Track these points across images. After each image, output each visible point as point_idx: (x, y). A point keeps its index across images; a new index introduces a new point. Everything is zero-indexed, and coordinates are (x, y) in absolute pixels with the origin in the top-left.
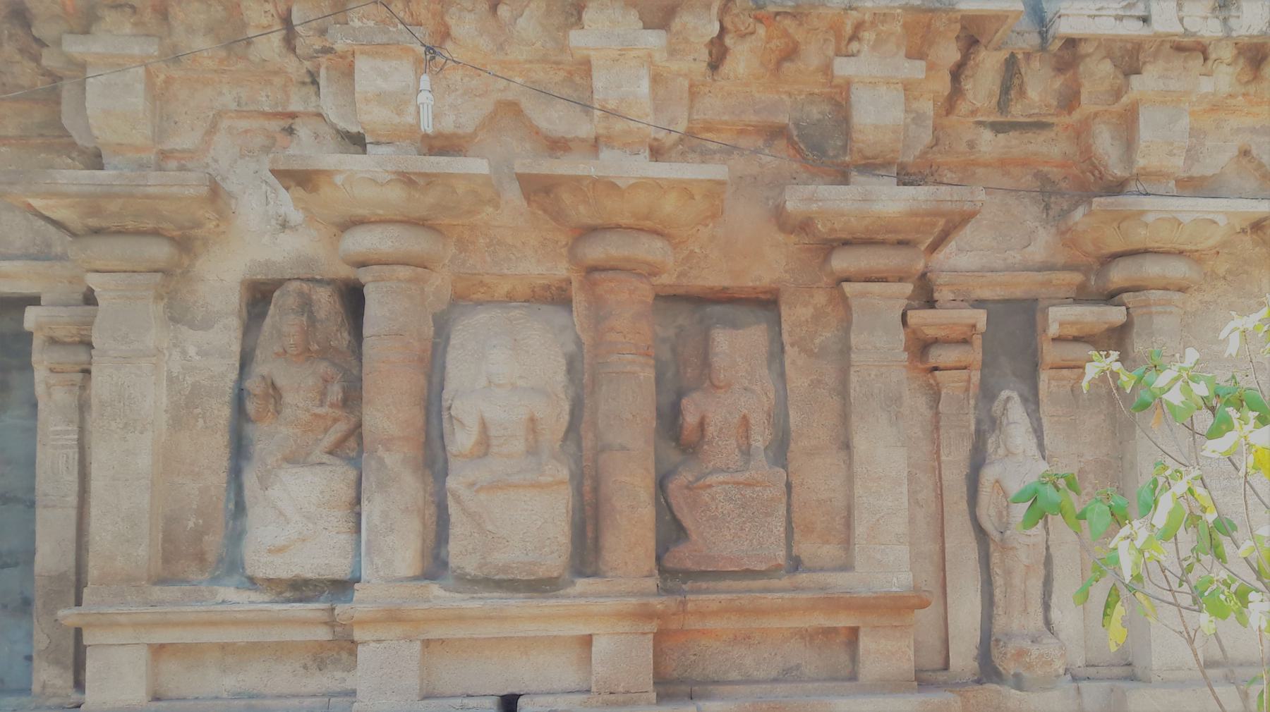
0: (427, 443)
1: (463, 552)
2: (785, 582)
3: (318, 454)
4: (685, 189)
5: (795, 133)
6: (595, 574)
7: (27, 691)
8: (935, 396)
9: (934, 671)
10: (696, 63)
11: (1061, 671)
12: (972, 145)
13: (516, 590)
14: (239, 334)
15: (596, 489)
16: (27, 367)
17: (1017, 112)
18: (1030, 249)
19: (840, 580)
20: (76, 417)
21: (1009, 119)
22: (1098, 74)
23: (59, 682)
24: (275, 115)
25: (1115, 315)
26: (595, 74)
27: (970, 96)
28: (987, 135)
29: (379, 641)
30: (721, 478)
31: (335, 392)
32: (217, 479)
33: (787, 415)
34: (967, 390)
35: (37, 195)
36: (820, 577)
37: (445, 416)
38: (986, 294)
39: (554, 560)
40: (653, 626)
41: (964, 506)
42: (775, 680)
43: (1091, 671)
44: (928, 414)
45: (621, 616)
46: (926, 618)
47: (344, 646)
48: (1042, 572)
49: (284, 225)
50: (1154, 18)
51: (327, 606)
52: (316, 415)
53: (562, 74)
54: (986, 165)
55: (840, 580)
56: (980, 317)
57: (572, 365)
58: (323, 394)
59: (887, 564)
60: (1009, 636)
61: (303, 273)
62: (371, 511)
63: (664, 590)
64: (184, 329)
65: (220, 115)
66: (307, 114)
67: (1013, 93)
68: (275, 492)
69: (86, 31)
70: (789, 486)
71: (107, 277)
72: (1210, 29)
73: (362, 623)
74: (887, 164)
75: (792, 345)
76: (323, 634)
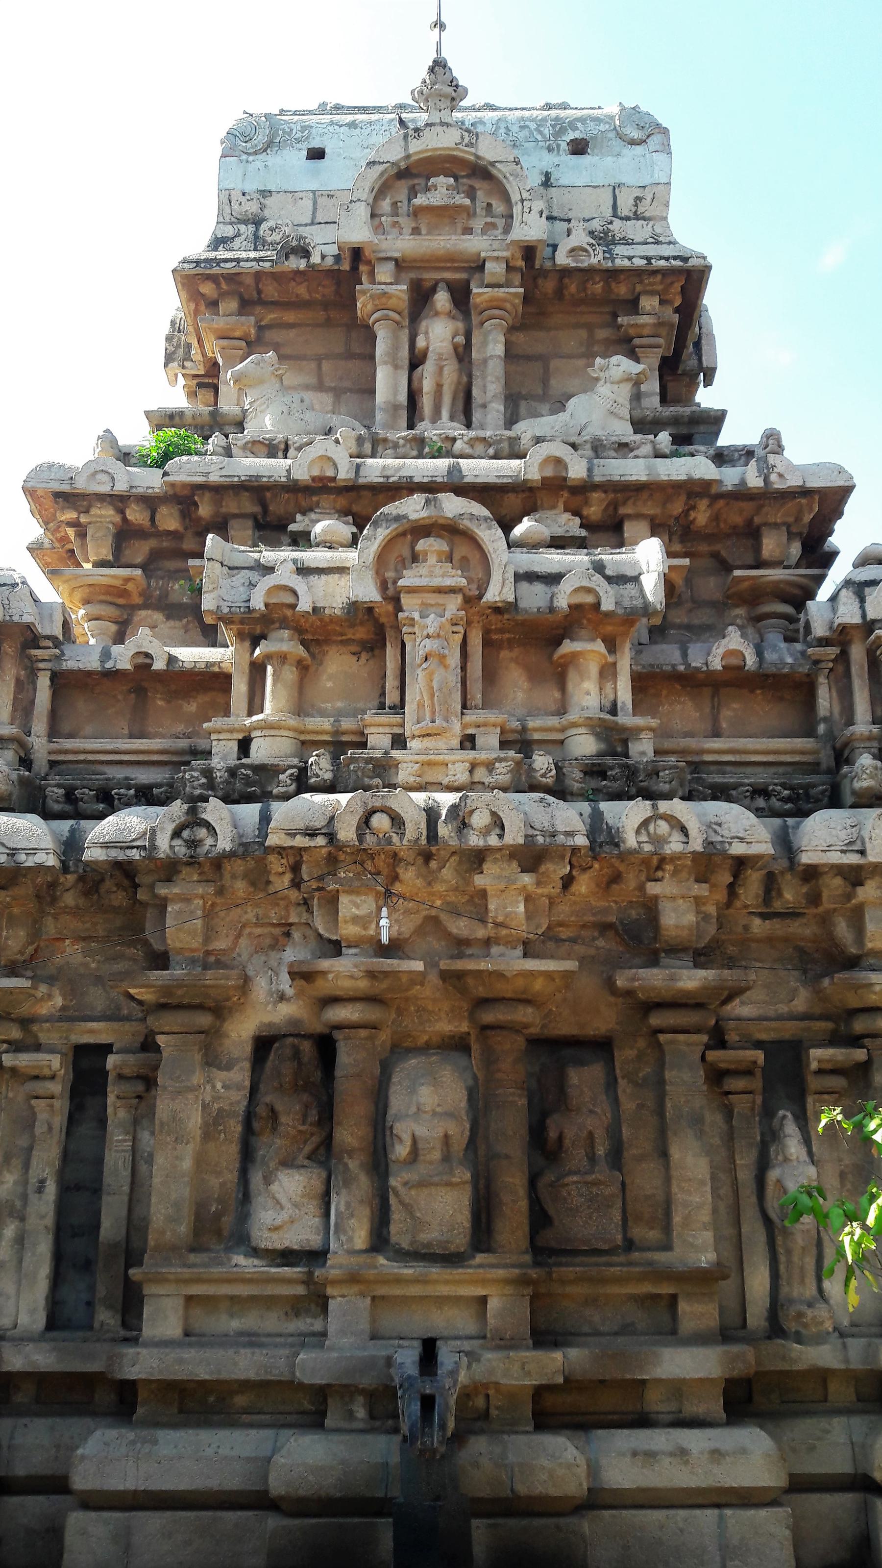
0: (375, 1152)
1: (399, 1231)
2: (622, 1259)
3: (301, 1160)
4: (548, 975)
5: (620, 928)
6: (488, 1250)
7: (91, 1328)
8: (729, 1113)
9: (736, 1329)
10: (553, 888)
11: (830, 1329)
12: (746, 928)
13: (435, 1262)
14: (249, 1074)
15: (488, 1187)
16: (105, 1095)
17: (778, 906)
18: (794, 1003)
19: (661, 1257)
20: (132, 1129)
21: (772, 910)
22: (834, 885)
23: (112, 1322)
24: (279, 925)
25: (860, 1055)
26: (490, 900)
27: (742, 897)
28: (757, 921)
29: (343, 1296)
30: (575, 1179)
31: (313, 1115)
32: (231, 1177)
33: (620, 1131)
34: (753, 1109)
35: (136, 987)
36: (649, 1255)
37: (388, 1133)
38: (764, 1036)
39: (460, 1241)
40: (529, 1291)
41: (754, 1199)
42: (616, 1334)
43: (855, 1330)
44: (725, 1127)
45: (507, 1282)
46: (728, 1286)
47: (318, 1301)
48: (814, 1251)
49: (282, 997)
50: (869, 851)
51: (305, 1269)
52: (300, 1132)
53: (467, 897)
54: (758, 941)
55: (661, 1257)
56: (759, 1056)
57: (472, 1094)
58: (305, 1116)
59: (698, 1245)
60: (791, 1301)
61: (292, 1030)
62: (338, 1203)
63: (537, 1264)
64: (215, 1070)
65: (244, 926)
66: (300, 924)
67: (774, 894)
68: (274, 1187)
69: (169, 880)
70: (623, 1184)
71: (170, 1037)
73: (335, 1282)
74: (684, 950)
75: (623, 1078)
76: (301, 1290)
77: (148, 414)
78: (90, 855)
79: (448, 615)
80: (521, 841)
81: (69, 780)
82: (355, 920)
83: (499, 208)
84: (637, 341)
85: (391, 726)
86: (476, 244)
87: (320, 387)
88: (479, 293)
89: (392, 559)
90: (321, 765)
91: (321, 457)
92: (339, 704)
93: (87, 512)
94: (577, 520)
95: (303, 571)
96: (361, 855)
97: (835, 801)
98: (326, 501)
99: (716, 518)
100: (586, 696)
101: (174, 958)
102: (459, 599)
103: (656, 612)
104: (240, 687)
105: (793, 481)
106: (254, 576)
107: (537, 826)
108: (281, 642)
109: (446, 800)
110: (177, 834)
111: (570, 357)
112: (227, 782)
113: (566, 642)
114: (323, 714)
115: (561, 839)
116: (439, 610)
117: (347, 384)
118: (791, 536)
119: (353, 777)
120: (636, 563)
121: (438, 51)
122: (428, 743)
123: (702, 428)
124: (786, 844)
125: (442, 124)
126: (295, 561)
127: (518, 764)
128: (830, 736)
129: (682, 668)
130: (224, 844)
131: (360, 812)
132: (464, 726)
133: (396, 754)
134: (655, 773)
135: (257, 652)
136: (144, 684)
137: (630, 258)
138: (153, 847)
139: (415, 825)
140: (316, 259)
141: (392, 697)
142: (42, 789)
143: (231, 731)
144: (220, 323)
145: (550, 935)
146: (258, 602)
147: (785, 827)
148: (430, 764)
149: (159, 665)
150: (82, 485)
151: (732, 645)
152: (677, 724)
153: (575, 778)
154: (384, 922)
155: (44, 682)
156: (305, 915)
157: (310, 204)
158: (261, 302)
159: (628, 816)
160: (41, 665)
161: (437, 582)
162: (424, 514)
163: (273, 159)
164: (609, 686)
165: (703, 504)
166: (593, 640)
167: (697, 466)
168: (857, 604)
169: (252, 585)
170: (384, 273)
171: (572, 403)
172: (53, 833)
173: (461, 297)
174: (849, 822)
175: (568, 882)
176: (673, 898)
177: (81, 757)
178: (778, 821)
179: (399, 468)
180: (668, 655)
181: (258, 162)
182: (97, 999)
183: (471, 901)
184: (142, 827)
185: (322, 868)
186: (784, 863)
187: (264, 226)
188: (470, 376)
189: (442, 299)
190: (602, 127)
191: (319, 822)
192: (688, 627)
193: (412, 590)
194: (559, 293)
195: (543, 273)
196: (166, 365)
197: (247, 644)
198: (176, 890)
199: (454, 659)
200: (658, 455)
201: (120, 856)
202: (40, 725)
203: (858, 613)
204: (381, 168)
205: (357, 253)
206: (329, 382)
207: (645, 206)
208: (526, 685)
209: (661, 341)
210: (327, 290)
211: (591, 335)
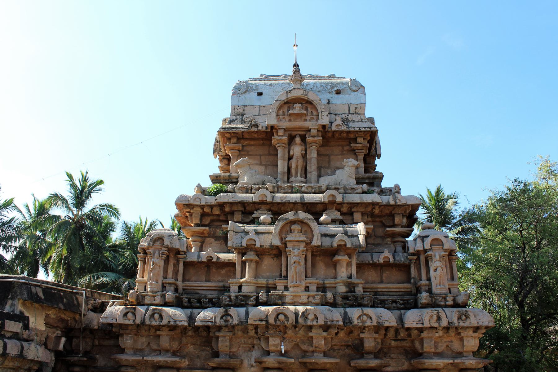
4: (331, 363)
12: (390, 344)
17: (399, 337)
28: (393, 342)
49: (252, 366)
54: (394, 347)
72: (436, 325)
77: (210, 176)
78: (197, 323)
79: (301, 249)
80: (323, 323)
81: (189, 296)
82: (274, 345)
83: (315, 113)
84: (357, 151)
85: (284, 283)
86: (308, 124)
87: (261, 164)
88: (309, 139)
89: (284, 231)
90: (263, 296)
91: (262, 194)
92: (268, 274)
93: (193, 209)
94: (339, 213)
95: (257, 233)
96: (276, 327)
97: (416, 306)
98: (263, 207)
99: (381, 211)
100: (343, 273)
101: (221, 354)
102: (304, 244)
103: (363, 247)
104: (238, 268)
105: (403, 202)
106: (243, 235)
107: (328, 318)
108: (251, 256)
109: (301, 309)
110: (222, 318)
111: (337, 155)
112: (235, 300)
113: (336, 256)
114: (264, 278)
115: (335, 322)
116: (298, 247)
117: (269, 163)
118: (403, 216)
119: (273, 300)
120: (357, 231)
121: (296, 42)
122: (295, 289)
123: (377, 180)
124: (401, 320)
125: (298, 89)
126: (255, 230)
127: (322, 296)
128: (415, 283)
129: (371, 262)
130: (236, 321)
131: (275, 314)
132: (306, 284)
133: (285, 293)
134: (363, 298)
135: (244, 258)
136: (211, 265)
137: (354, 128)
138: (215, 322)
139: (292, 319)
140: (260, 128)
141: (284, 273)
142: (182, 299)
143: (236, 283)
144: (232, 146)
145: (332, 349)
146: (244, 244)
147: (401, 314)
148: (295, 296)
149: (214, 260)
150: (192, 202)
151: (385, 255)
152: (370, 279)
153: (339, 300)
154: (282, 347)
155: (181, 265)
156: (259, 342)
157: (258, 109)
158: (243, 138)
159: (354, 313)
160: (181, 260)
161: (297, 239)
162: (294, 218)
163: (247, 95)
164: (349, 269)
165: (377, 207)
166: (344, 255)
167: (374, 197)
168: (422, 244)
169: (242, 238)
170: (281, 133)
171: (338, 172)
172: (186, 314)
173: (303, 138)
174: (419, 314)
175: (337, 334)
176: (368, 338)
177: (192, 288)
178: (398, 312)
179: (285, 198)
180: (367, 257)
181: (243, 96)
182: (198, 363)
183: (308, 339)
184: (212, 315)
185: (266, 328)
186: (401, 326)
187: (245, 116)
188: (306, 163)
189: (298, 140)
190: (345, 86)
191: (263, 317)
192: (373, 244)
193: (290, 241)
194: (333, 136)
195: (328, 131)
196: (214, 153)
197: (241, 255)
198: (221, 334)
199: (303, 263)
200: (364, 192)
201: (206, 324)
202: (180, 278)
203: (422, 246)
204: (280, 102)
205: (272, 127)
206: (263, 163)
207: (359, 110)
208: (324, 268)
209: (364, 151)
210: (264, 136)
211: (343, 148)
